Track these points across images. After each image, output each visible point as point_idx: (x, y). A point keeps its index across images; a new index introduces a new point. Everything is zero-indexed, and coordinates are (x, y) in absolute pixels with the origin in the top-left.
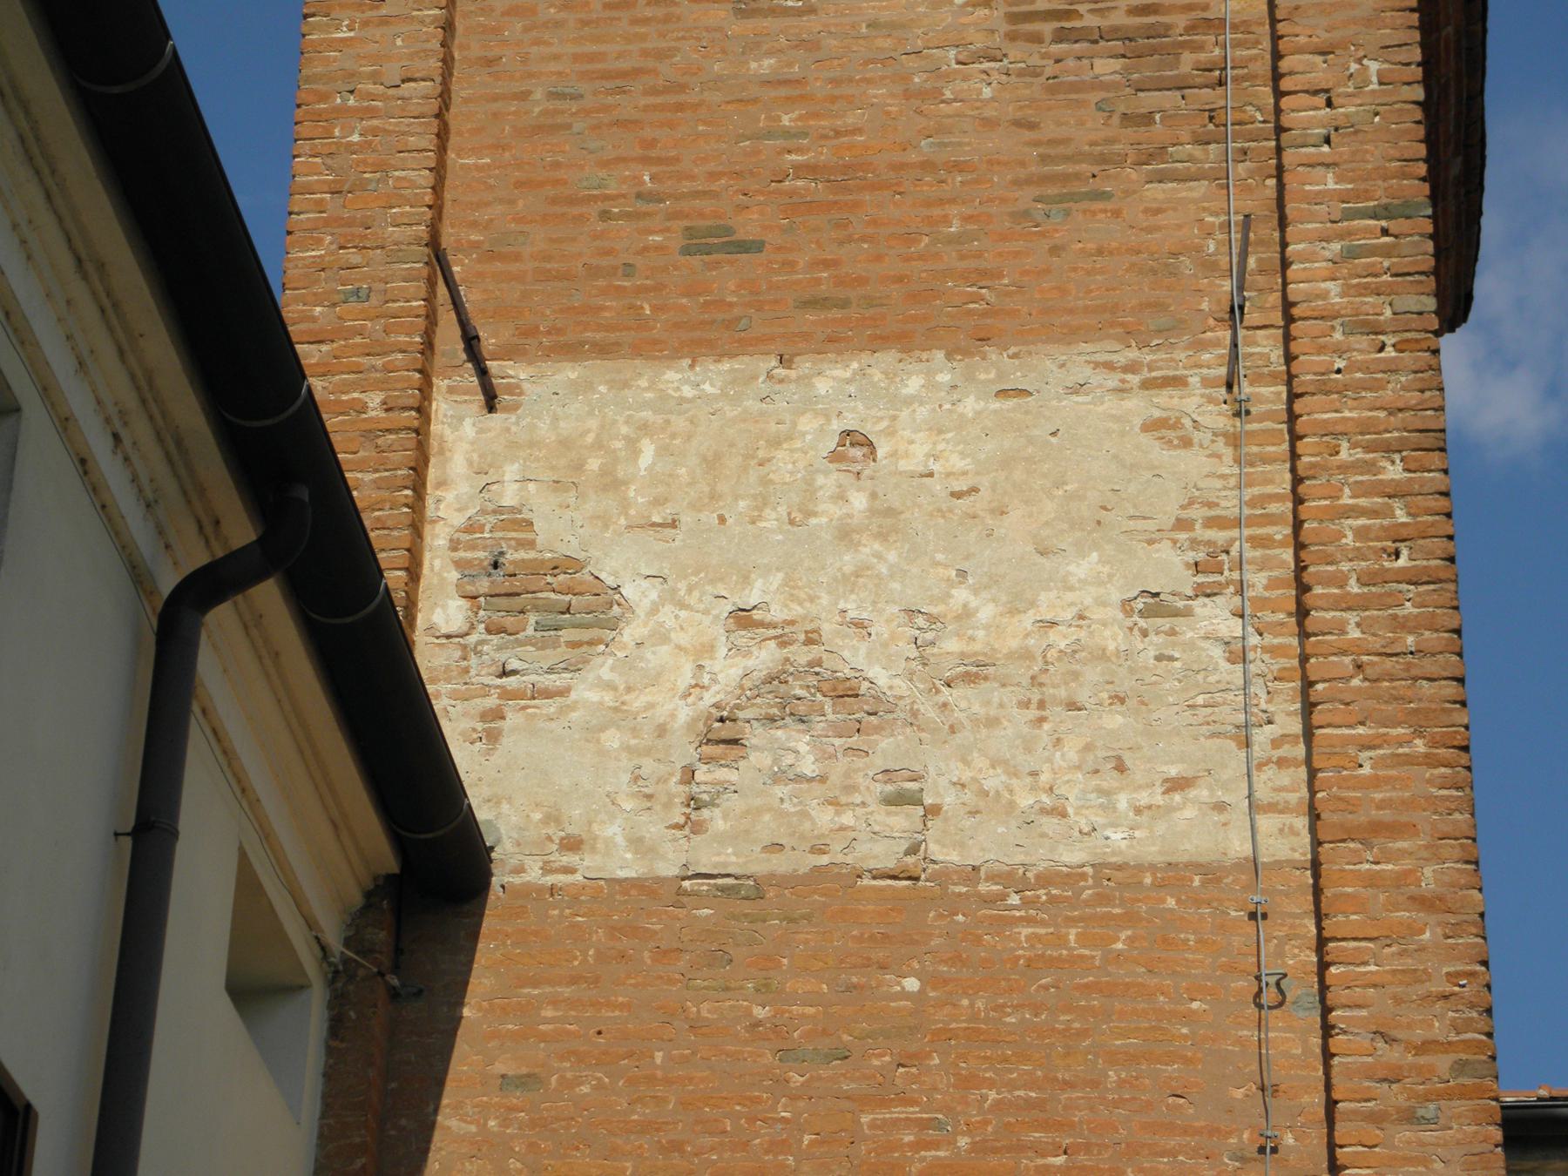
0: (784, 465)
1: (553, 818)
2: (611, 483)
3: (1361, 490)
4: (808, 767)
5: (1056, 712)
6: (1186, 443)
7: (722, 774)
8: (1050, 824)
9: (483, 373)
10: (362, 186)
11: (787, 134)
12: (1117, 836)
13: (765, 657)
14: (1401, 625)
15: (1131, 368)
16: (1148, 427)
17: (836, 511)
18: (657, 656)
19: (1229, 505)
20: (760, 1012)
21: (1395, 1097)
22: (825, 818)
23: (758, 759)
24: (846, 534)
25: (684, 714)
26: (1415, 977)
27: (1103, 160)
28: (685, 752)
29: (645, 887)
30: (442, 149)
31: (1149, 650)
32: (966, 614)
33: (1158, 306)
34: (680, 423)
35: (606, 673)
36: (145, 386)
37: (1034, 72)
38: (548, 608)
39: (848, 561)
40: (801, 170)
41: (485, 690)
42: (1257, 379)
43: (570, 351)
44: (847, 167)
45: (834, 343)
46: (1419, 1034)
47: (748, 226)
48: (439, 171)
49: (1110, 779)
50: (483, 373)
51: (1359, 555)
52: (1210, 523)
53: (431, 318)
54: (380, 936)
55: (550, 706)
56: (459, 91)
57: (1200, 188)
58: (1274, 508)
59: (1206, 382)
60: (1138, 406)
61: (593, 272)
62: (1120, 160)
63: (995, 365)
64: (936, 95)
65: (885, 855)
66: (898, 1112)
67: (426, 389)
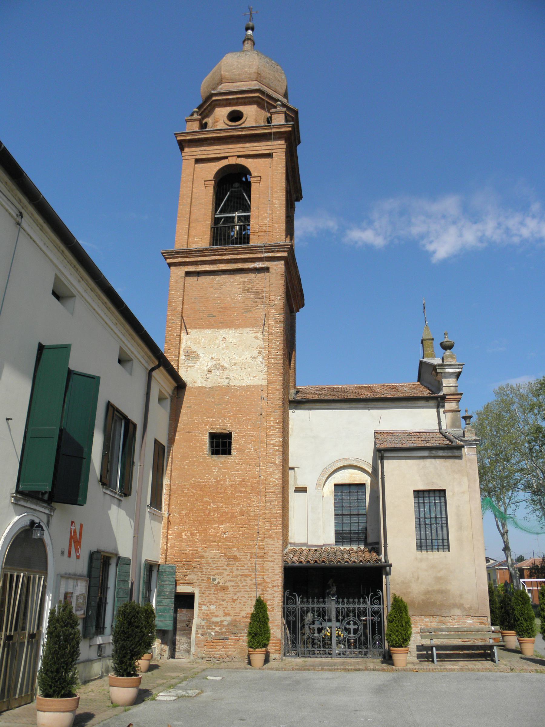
0: (217, 341)
1: (193, 380)
2: (199, 343)
3: (275, 346)
4: (218, 374)
5: (243, 369)
6: (258, 339)
7: (210, 375)
8: (242, 381)
9: (187, 331)
10: (174, 310)
11: (219, 303)
12: (248, 382)
13: (214, 362)
14: (277, 360)
15: (253, 331)
16: (254, 337)
17: (222, 346)
18: (203, 362)
19: (262, 346)
20: (213, 400)
21: (273, 410)
22: (220, 380)
23: (213, 374)
24: (223, 349)
25: (206, 369)
26: (275, 398)
27: (251, 307)
28: (206, 373)
29: (202, 387)
30: (183, 305)
31: (253, 362)
32: (235, 358)
33: (256, 324)
34: (207, 336)
35: (198, 364)
36: (146, 353)
37: (245, 296)
38: (192, 357)
39: (223, 352)
40: (220, 308)
41: (186, 366)
42: (265, 332)
43: (195, 328)
44: (225, 307)
45: (223, 327)
46: (276, 403)
47: (214, 314)
48: (182, 308)
49: (248, 376)
50: (187, 331)
51: (274, 353)
52: (260, 348)
53: (181, 325)
54: (176, 392)
55: (193, 367)
56: (185, 298)
57: (261, 310)
58: (266, 347)
59: (260, 332)
60: (253, 335)
61: (198, 319)
62: (253, 307)
63: (239, 330)
64: (234, 299)
65: (225, 384)
66: (226, 411)
67: (181, 333)
